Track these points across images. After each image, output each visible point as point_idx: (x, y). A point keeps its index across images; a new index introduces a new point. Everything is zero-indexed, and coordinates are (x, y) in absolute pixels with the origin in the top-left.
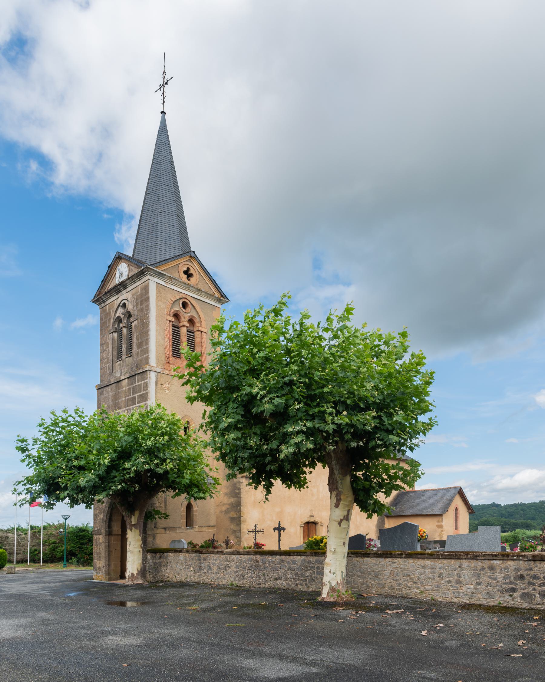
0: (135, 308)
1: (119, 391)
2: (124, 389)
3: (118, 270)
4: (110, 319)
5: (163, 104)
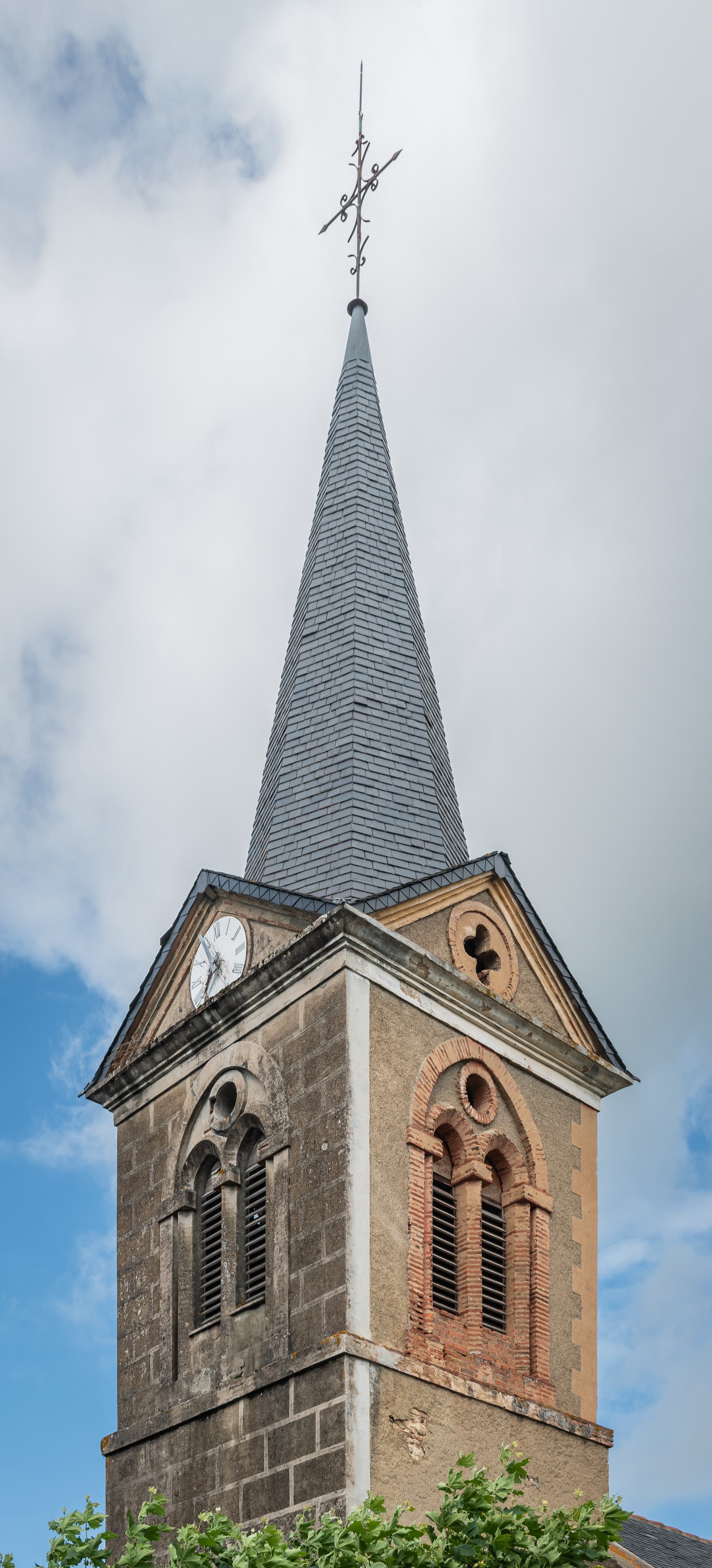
0: (280, 1097)
1: (210, 1453)
2: (232, 1443)
3: (201, 948)
4: (163, 1158)
5: (356, 271)
